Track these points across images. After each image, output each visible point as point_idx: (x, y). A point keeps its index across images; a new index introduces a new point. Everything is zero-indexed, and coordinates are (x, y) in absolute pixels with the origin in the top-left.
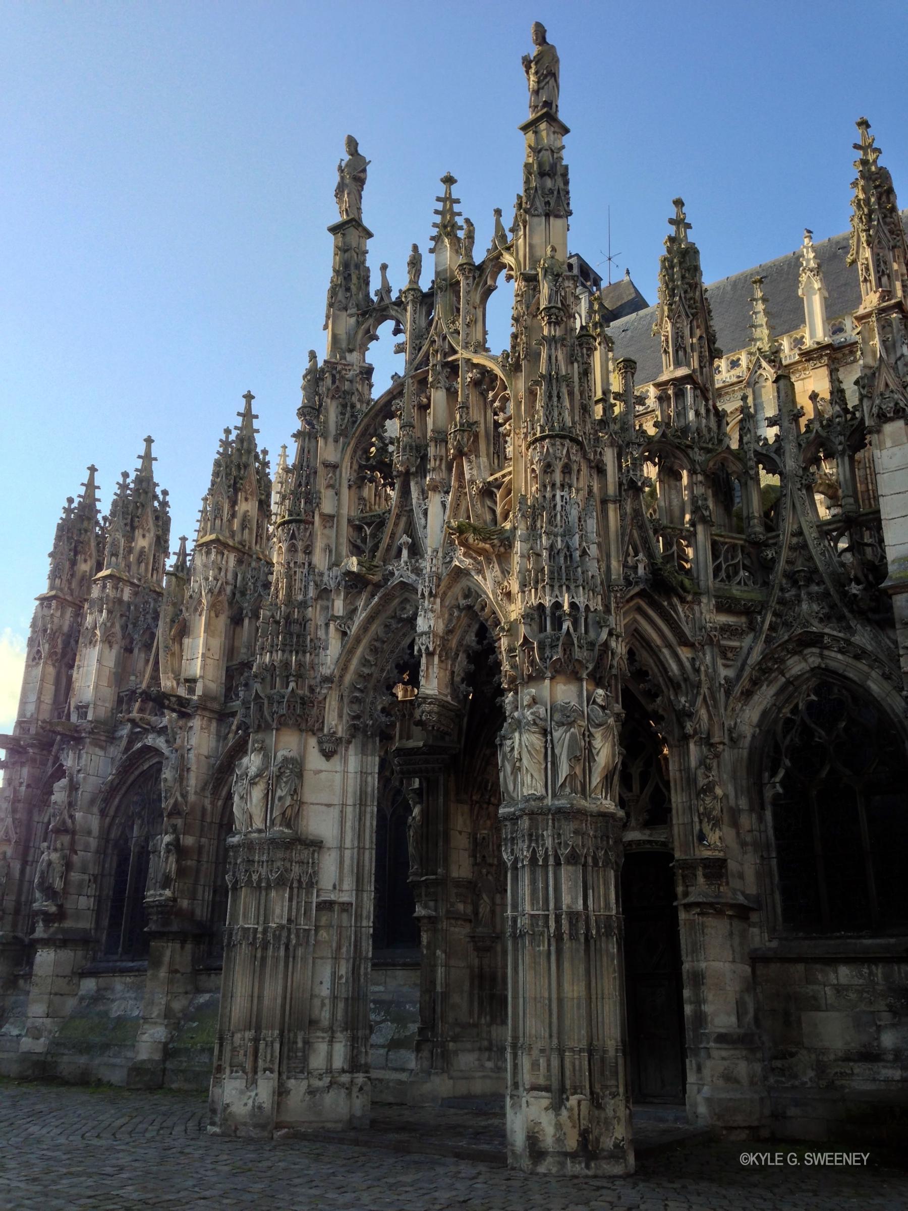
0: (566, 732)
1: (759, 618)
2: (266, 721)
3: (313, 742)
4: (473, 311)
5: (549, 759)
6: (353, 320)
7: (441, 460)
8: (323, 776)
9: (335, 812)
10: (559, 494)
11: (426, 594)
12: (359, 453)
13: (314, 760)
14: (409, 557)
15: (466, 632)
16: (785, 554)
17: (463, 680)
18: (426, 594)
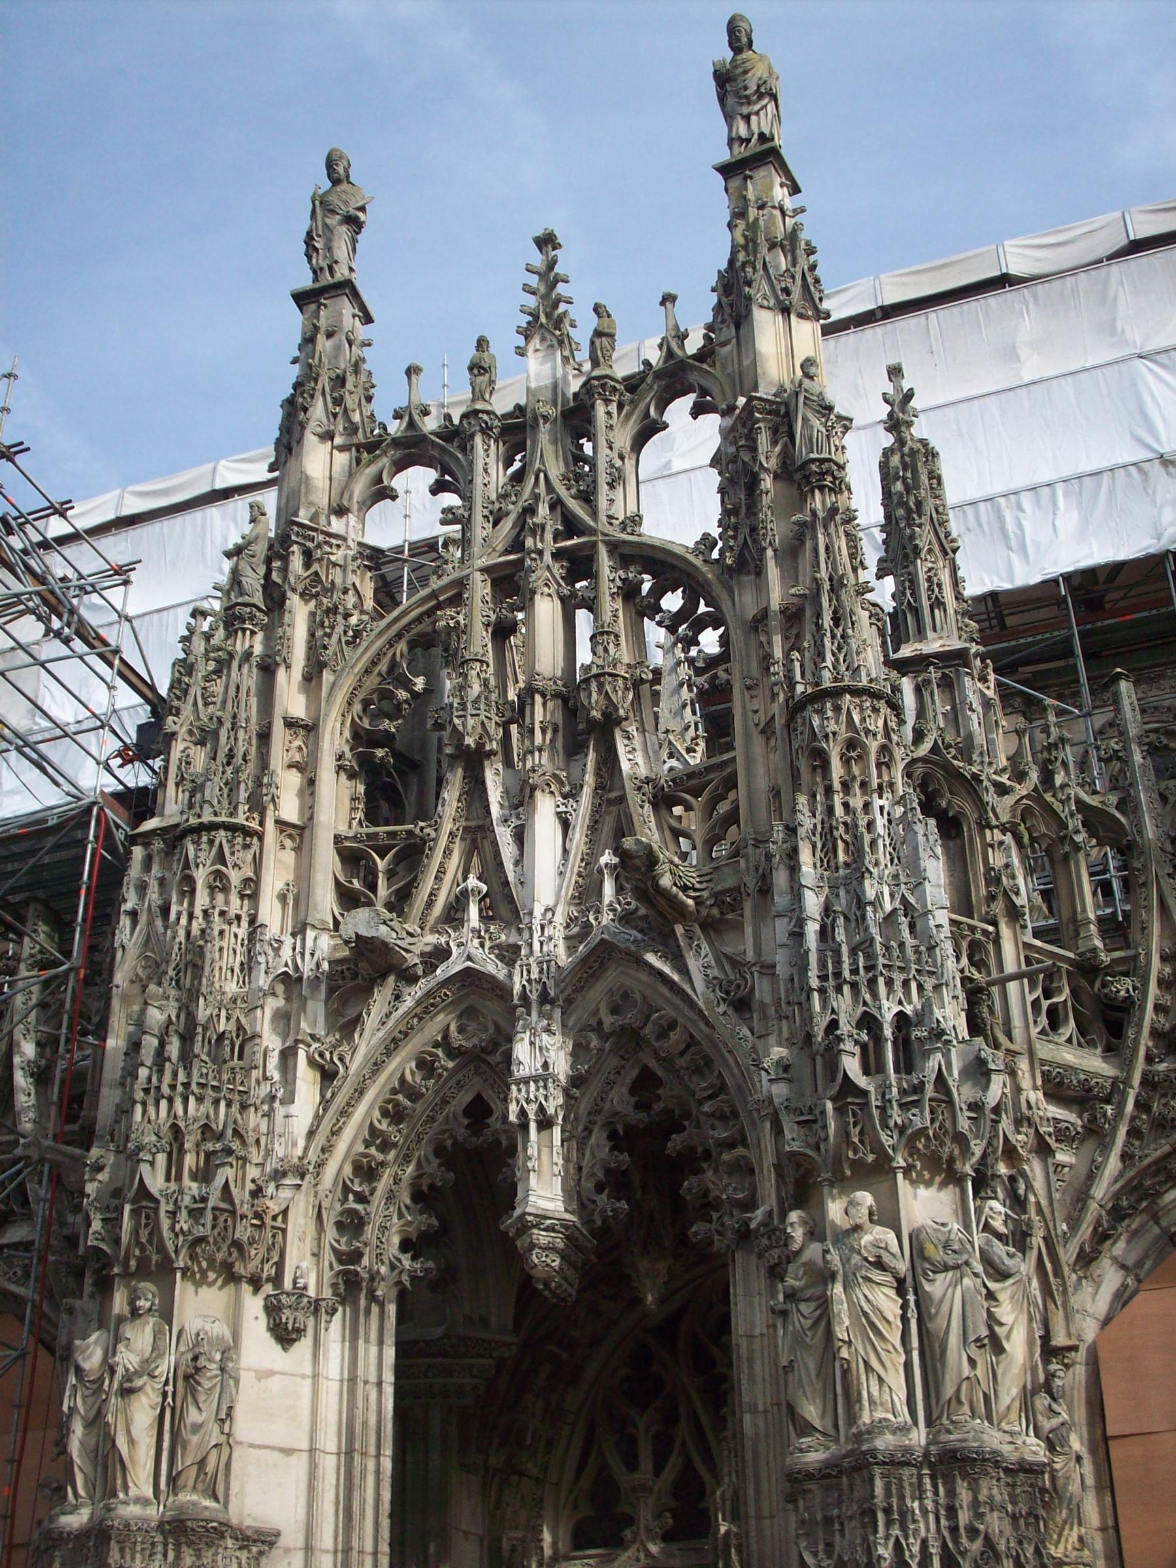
0: (953, 1285)
1: (1109, 1109)
2: (162, 1249)
3: (253, 1305)
4: (618, 463)
5: (915, 1343)
6: (342, 459)
7: (555, 731)
8: (275, 1382)
9: (300, 1464)
10: (877, 802)
11: (534, 996)
12: (357, 707)
13: (257, 1345)
14: (483, 918)
15: (610, 1083)
16: (1153, 989)
17: (599, 1188)
18: (534, 996)
